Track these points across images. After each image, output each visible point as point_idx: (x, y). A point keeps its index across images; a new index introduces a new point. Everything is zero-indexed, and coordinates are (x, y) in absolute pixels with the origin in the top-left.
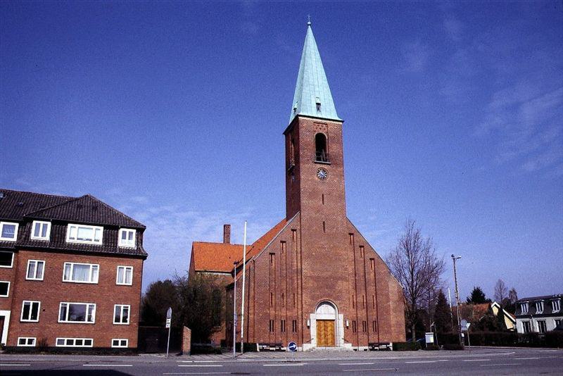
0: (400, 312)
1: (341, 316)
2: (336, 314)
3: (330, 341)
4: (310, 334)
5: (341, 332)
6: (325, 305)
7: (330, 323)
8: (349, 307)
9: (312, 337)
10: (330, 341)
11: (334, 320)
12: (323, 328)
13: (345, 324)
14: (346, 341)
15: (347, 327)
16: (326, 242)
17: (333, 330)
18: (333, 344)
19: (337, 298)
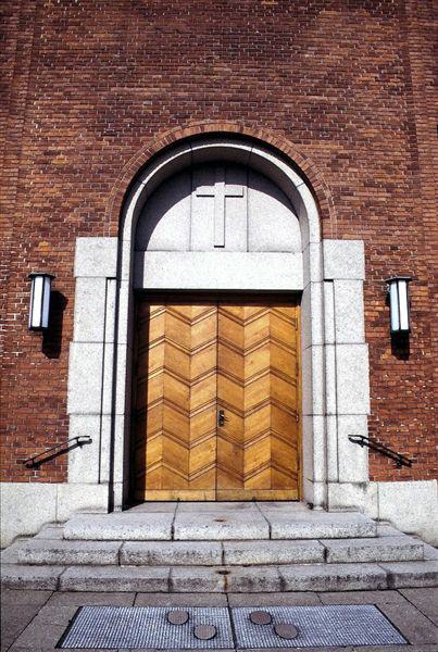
0: (46, 623)
1: (348, 258)
2: (306, 248)
3: (258, 454)
4: (58, 403)
5: (344, 387)
6: (220, 188)
7: (260, 322)
8: (414, 190)
9: (77, 428)
10: (258, 454)
11: (292, 298)
12: (206, 359)
13: (377, 320)
14: (388, 458)
15: (400, 342)
16: (420, 330)
17: (290, 372)
18: (288, 478)
19: (314, 124)
